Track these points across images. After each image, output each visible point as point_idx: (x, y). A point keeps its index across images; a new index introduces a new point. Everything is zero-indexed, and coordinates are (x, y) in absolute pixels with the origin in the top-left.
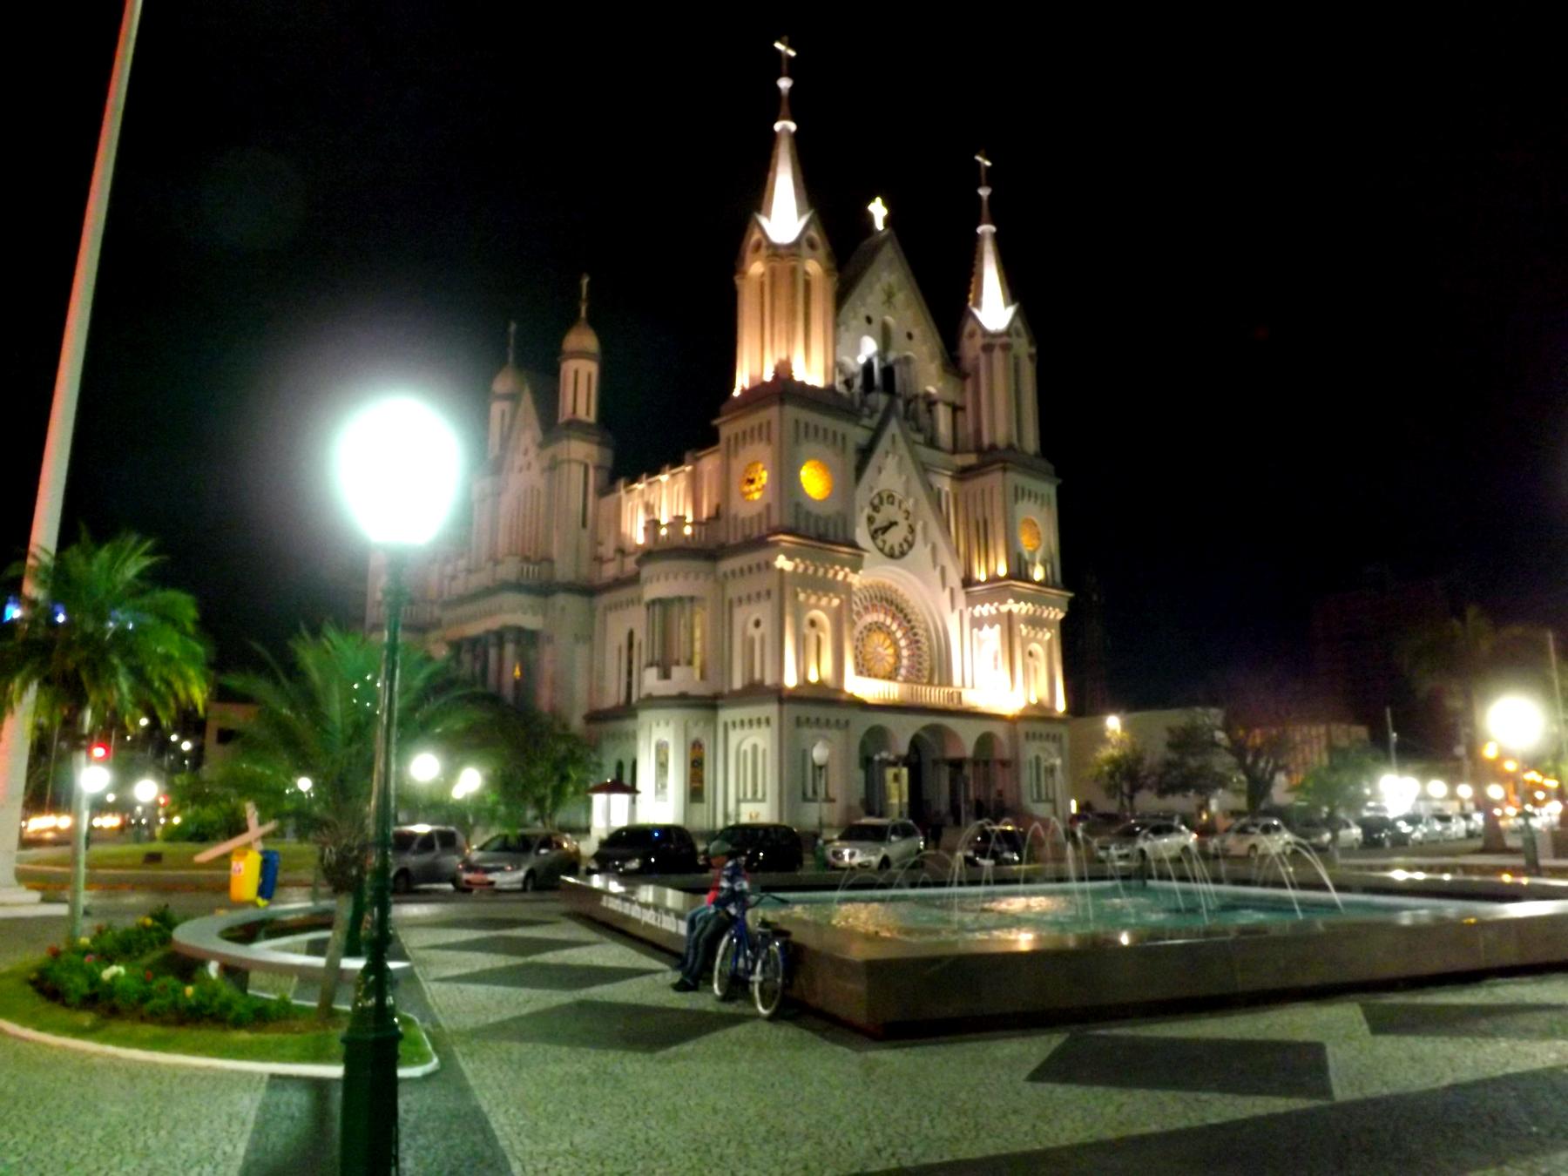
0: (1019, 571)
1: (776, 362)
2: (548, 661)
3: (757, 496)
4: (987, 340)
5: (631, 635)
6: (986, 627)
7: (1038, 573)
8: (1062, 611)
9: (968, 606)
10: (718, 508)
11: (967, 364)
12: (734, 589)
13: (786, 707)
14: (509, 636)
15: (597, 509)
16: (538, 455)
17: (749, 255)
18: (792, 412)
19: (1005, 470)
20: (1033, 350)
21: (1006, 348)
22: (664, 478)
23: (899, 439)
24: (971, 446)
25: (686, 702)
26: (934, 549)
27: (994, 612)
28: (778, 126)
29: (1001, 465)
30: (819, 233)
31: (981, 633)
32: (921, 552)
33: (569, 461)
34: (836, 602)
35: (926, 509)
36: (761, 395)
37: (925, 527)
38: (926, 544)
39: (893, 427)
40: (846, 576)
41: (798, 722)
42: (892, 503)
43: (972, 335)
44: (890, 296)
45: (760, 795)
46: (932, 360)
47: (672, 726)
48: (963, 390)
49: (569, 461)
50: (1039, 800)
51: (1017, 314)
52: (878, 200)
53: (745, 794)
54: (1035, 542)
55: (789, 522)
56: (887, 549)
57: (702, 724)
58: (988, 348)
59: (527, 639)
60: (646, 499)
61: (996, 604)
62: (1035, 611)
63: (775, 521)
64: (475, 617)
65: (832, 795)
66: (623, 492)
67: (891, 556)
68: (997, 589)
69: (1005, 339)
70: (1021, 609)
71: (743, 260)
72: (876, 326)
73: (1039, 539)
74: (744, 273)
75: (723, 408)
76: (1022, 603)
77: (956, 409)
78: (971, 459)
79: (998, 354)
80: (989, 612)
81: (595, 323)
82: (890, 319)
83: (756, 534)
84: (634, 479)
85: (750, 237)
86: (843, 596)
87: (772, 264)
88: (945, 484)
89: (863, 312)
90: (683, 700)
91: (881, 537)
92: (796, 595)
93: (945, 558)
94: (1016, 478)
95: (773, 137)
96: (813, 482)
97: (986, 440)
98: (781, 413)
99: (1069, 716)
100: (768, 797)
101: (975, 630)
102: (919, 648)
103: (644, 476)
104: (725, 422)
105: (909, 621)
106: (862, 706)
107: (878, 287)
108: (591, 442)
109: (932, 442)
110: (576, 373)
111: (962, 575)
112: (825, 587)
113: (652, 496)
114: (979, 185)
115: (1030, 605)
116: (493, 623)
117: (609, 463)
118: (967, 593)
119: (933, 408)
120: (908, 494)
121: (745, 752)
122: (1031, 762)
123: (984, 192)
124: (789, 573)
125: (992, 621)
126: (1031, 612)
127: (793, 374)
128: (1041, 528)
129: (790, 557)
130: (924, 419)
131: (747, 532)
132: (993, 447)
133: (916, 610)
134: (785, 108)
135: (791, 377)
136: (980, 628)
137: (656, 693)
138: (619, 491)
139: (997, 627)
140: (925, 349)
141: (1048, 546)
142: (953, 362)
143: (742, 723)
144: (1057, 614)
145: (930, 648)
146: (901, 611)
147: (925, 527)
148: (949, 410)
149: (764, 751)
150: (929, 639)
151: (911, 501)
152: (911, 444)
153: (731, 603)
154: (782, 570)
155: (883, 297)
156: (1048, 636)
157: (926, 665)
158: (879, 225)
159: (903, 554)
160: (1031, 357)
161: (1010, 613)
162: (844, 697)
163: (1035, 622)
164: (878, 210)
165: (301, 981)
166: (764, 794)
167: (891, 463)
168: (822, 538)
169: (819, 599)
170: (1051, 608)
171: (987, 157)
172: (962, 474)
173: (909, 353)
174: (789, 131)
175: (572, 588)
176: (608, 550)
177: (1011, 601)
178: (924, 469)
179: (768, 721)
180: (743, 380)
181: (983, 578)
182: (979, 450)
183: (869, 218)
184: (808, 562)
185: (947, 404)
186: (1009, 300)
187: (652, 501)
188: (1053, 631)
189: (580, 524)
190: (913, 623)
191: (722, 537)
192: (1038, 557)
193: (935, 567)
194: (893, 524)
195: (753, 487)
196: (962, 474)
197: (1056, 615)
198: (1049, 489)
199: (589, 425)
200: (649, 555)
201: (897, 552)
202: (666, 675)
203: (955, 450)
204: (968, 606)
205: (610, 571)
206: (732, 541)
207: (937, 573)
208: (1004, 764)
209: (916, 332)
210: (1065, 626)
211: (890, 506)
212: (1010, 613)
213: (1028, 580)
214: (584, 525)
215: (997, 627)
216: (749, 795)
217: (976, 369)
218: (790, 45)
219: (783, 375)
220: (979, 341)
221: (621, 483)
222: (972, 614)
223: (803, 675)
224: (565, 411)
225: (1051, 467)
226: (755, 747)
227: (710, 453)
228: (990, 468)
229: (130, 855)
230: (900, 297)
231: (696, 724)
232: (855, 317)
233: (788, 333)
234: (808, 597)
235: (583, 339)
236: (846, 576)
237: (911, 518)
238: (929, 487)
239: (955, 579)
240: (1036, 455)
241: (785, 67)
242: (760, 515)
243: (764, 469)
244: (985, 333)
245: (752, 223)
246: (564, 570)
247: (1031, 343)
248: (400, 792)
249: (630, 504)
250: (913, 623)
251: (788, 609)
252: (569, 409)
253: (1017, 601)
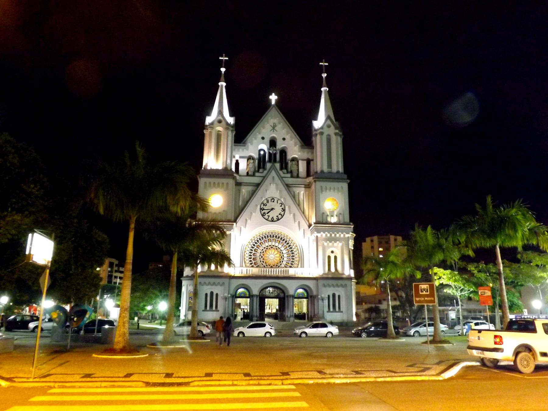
23: (276, 178)
28: (220, 84)
32: (288, 216)
35: (289, 201)
37: (289, 207)
38: (290, 213)
39: (273, 173)
44: (274, 128)
52: (273, 94)
56: (270, 219)
67: (272, 220)
70: (322, 235)
72: (267, 140)
77: (309, 162)
88: (301, 192)
89: (260, 136)
91: (267, 215)
95: (321, 91)
114: (322, 73)
115: (322, 233)
122: (206, 295)
123: (223, 70)
130: (294, 168)
134: (223, 78)
147: (289, 207)
151: (282, 200)
152: (281, 178)
155: (272, 128)
156: (340, 244)
157: (297, 259)
158: (273, 102)
159: (278, 220)
160: (336, 134)
163: (330, 239)
164: (273, 98)
165: (111, 342)
167: (273, 187)
169: (333, 244)
173: (284, 146)
178: (288, 186)
183: (270, 101)
185: (303, 160)
192: (335, 213)
194: (272, 209)
196: (308, 186)
198: (345, 186)
201: (275, 219)
211: (272, 203)
218: (226, 56)
230: (279, 127)
231: (190, 285)
232: (256, 138)
237: (283, 206)
248: (3, 311)
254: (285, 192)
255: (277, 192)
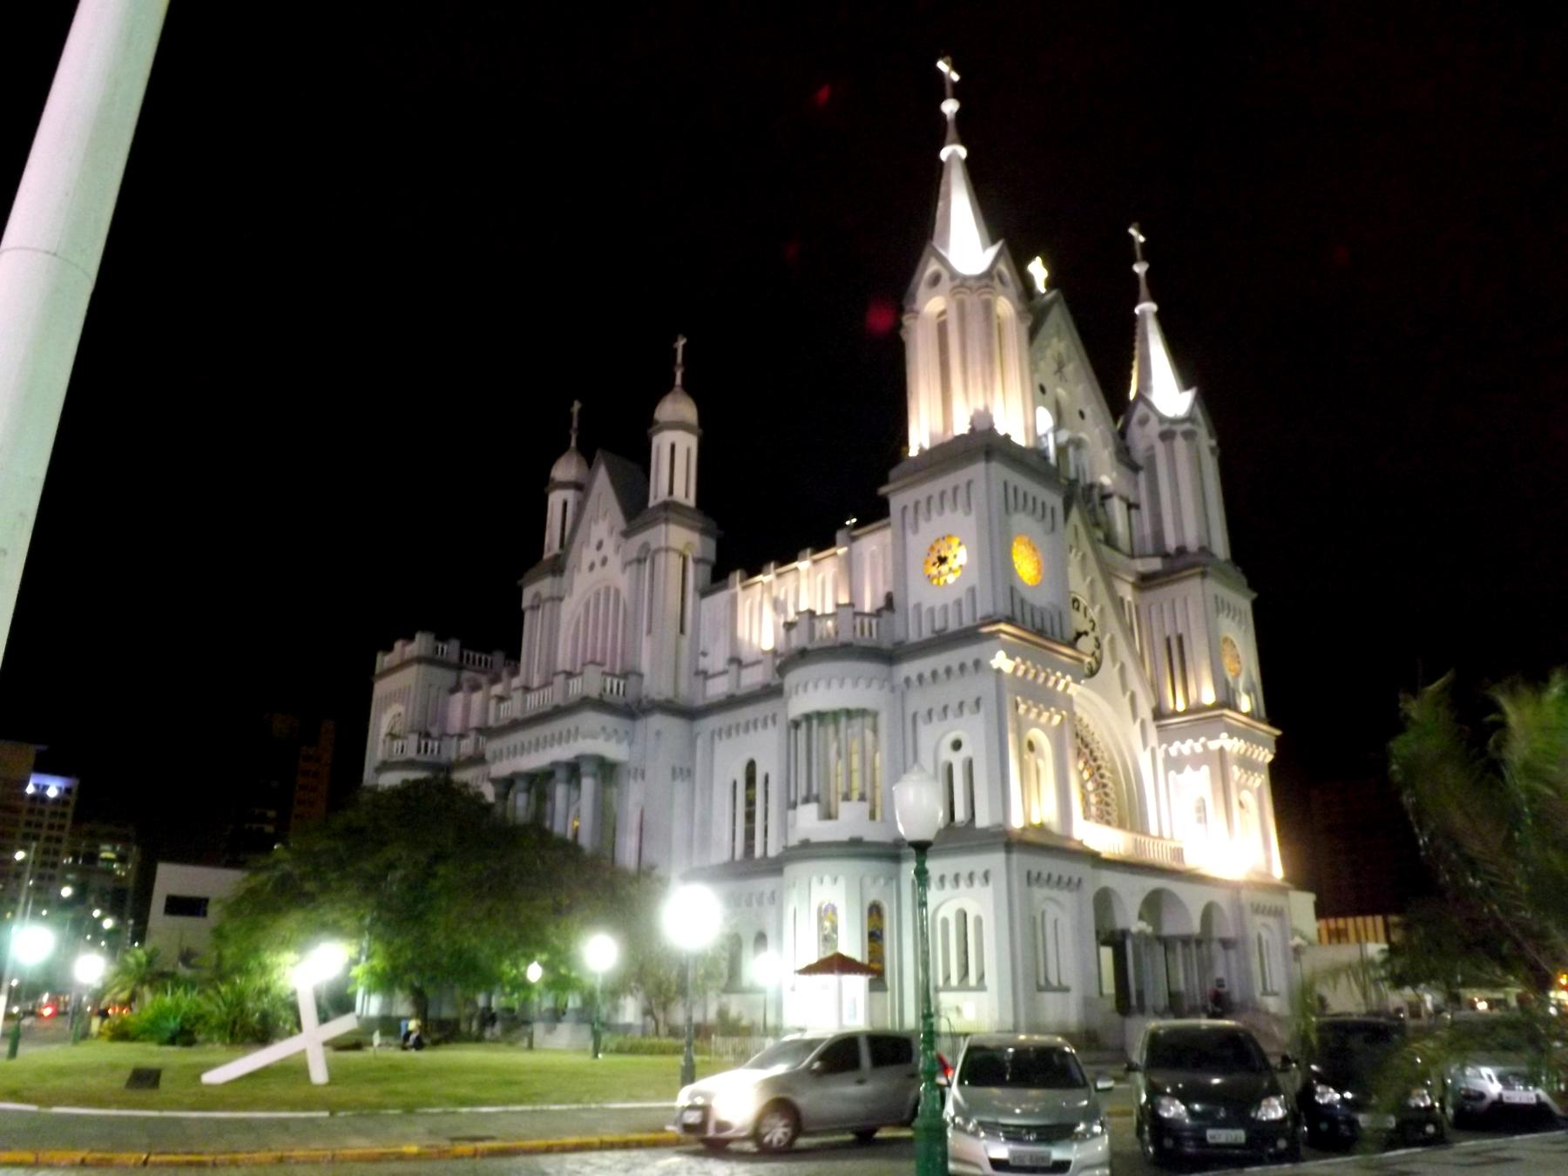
0: (1227, 701)
1: (972, 413)
2: (633, 798)
3: (951, 579)
4: (1166, 427)
5: (751, 766)
6: (1188, 769)
7: (1245, 703)
8: (1270, 752)
9: (1160, 744)
10: (889, 599)
11: (1139, 455)
12: (918, 701)
13: (1015, 857)
14: (585, 768)
15: (697, 611)
16: (618, 548)
17: (922, 290)
18: (999, 471)
19: (1204, 575)
20: (1213, 443)
21: (1189, 435)
22: (803, 565)
23: (1081, 530)
24: (1149, 548)
25: (860, 850)
26: (1122, 669)
27: (1199, 748)
28: (944, 154)
29: (1198, 570)
30: (1008, 268)
31: (1180, 777)
32: (1109, 671)
33: (667, 550)
34: (1057, 719)
36: (950, 455)
37: (1112, 640)
40: (1067, 686)
41: (1032, 879)
42: (1078, 609)
43: (1144, 422)
45: (972, 979)
46: (1106, 446)
47: (842, 882)
48: (1136, 485)
49: (667, 550)
50: (1265, 993)
51: (1196, 399)
53: (947, 978)
54: (1237, 666)
55: (1003, 608)
57: (882, 881)
58: (1167, 436)
59: (607, 770)
60: (775, 593)
61: (1202, 740)
62: (1246, 750)
63: (984, 608)
64: (538, 745)
65: (1065, 982)
66: (738, 587)
68: (1202, 719)
69: (1187, 426)
70: (1234, 746)
71: (913, 298)
73: (1239, 662)
74: (916, 313)
75: (893, 473)
76: (1235, 739)
77: (1131, 506)
78: (1155, 564)
79: (1180, 443)
80: (1192, 749)
81: (690, 389)
82: (1061, 392)
83: (967, 622)
84: (753, 570)
85: (925, 269)
86: (1064, 713)
87: (959, 296)
88: (1126, 592)
90: (855, 848)
92: (1017, 707)
93: (1135, 683)
94: (1213, 587)
96: (1026, 566)
97: (1171, 543)
98: (987, 469)
99: (1287, 885)
100: (991, 979)
101: (1172, 774)
102: (1106, 795)
103: (772, 565)
104: (894, 491)
105: (1095, 760)
106: (1096, 860)
107: (1049, 353)
108: (692, 528)
109: (1110, 540)
110: (673, 447)
111: (1154, 704)
112: (1045, 698)
113: (783, 590)
116: (563, 753)
117: (712, 555)
118: (1158, 727)
119: (1108, 502)
120: (1093, 600)
121: (945, 922)
123: (1140, 268)
124: (1007, 674)
125: (1197, 761)
126: (1242, 751)
127: (996, 427)
128: (1240, 649)
129: (1011, 656)
131: (938, 625)
132: (1181, 551)
133: (1101, 745)
134: (952, 132)
135: (991, 430)
136: (1180, 771)
137: (814, 838)
138: (735, 585)
139: (1205, 769)
140: (1097, 431)
141: (1249, 676)
142: (1124, 454)
143: (971, 877)
144: (1265, 755)
145: (1118, 794)
146: (1087, 746)
147: (1112, 640)
148: (1124, 506)
149: (979, 921)
150: (1117, 783)
152: (1094, 542)
153: (915, 716)
154: (999, 671)
155: (1055, 367)
160: (1212, 450)
161: (1222, 750)
162: (1072, 845)
163: (1247, 764)
166: (981, 977)
168: (1040, 632)
170: (1261, 748)
171: (1142, 231)
172: (1145, 582)
174: (959, 158)
175: (671, 708)
176: (716, 660)
177: (1224, 735)
179: (986, 877)
180: (922, 431)
181: (1181, 707)
182: (1165, 556)
184: (1039, 666)
185: (1123, 499)
186: (884, 522)
187: (782, 597)
188: (1263, 776)
189: (678, 630)
190: (1099, 762)
191: (899, 634)
193: (1124, 693)
195: (944, 568)
196: (1145, 582)
197: (1265, 757)
198: (1244, 603)
199: (687, 508)
200: (793, 659)
202: (828, 815)
203: (1132, 556)
204: (1160, 744)
205: (718, 688)
206: (913, 637)
207: (1126, 700)
208: (1226, 944)
209: (1087, 412)
210: (1277, 771)
212: (1222, 750)
213: (1235, 708)
214: (682, 631)
215: (1205, 769)
216: (954, 981)
217: (1151, 459)
219: (981, 427)
220: (1154, 428)
221: (737, 576)
222: (1167, 752)
223: (1027, 815)
224: (658, 491)
225: (1244, 581)
226: (963, 916)
227: (879, 529)
228: (1186, 573)
229: (95, 1070)
231: (875, 880)
233: (983, 376)
234: (1028, 710)
235: (677, 408)
236: (1067, 686)
238: (1110, 588)
239: (1145, 711)
240: (1226, 561)
241: (949, 90)
242: (958, 603)
243: (960, 544)
244: (1162, 419)
245: (927, 250)
246: (656, 685)
247: (1211, 436)
249: (748, 602)
250: (1099, 762)
251: (1010, 724)
252: (1195, 696)
253: (1231, 737)
254: (1101, 587)
255: (1084, 579)
